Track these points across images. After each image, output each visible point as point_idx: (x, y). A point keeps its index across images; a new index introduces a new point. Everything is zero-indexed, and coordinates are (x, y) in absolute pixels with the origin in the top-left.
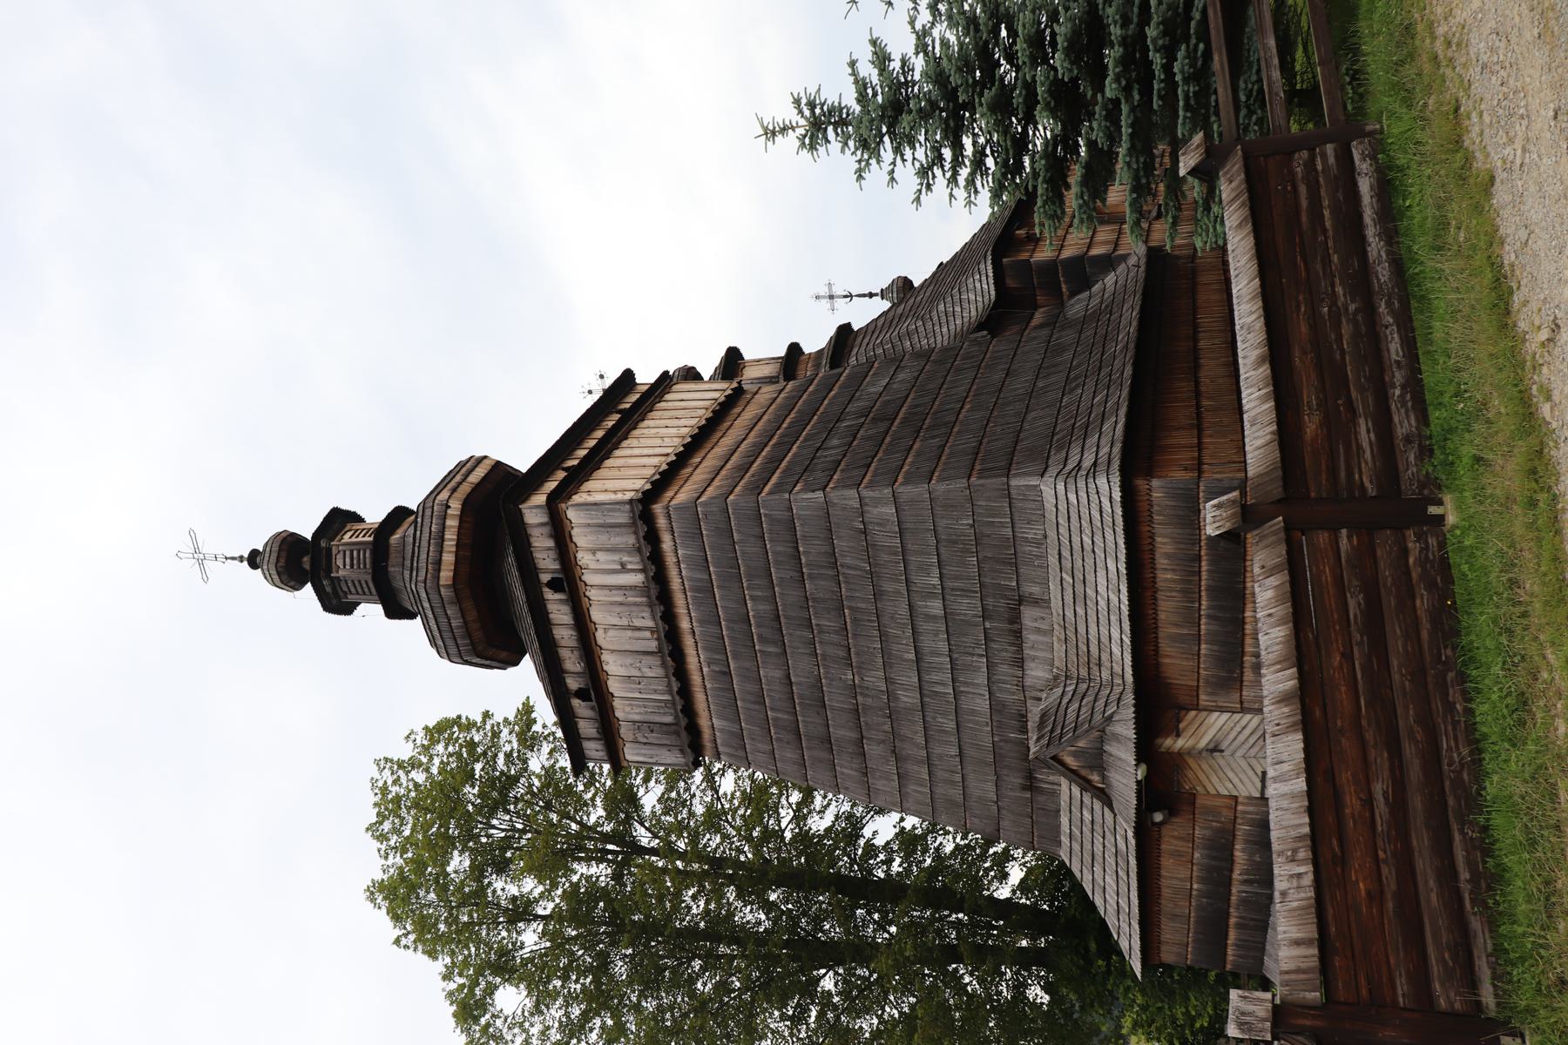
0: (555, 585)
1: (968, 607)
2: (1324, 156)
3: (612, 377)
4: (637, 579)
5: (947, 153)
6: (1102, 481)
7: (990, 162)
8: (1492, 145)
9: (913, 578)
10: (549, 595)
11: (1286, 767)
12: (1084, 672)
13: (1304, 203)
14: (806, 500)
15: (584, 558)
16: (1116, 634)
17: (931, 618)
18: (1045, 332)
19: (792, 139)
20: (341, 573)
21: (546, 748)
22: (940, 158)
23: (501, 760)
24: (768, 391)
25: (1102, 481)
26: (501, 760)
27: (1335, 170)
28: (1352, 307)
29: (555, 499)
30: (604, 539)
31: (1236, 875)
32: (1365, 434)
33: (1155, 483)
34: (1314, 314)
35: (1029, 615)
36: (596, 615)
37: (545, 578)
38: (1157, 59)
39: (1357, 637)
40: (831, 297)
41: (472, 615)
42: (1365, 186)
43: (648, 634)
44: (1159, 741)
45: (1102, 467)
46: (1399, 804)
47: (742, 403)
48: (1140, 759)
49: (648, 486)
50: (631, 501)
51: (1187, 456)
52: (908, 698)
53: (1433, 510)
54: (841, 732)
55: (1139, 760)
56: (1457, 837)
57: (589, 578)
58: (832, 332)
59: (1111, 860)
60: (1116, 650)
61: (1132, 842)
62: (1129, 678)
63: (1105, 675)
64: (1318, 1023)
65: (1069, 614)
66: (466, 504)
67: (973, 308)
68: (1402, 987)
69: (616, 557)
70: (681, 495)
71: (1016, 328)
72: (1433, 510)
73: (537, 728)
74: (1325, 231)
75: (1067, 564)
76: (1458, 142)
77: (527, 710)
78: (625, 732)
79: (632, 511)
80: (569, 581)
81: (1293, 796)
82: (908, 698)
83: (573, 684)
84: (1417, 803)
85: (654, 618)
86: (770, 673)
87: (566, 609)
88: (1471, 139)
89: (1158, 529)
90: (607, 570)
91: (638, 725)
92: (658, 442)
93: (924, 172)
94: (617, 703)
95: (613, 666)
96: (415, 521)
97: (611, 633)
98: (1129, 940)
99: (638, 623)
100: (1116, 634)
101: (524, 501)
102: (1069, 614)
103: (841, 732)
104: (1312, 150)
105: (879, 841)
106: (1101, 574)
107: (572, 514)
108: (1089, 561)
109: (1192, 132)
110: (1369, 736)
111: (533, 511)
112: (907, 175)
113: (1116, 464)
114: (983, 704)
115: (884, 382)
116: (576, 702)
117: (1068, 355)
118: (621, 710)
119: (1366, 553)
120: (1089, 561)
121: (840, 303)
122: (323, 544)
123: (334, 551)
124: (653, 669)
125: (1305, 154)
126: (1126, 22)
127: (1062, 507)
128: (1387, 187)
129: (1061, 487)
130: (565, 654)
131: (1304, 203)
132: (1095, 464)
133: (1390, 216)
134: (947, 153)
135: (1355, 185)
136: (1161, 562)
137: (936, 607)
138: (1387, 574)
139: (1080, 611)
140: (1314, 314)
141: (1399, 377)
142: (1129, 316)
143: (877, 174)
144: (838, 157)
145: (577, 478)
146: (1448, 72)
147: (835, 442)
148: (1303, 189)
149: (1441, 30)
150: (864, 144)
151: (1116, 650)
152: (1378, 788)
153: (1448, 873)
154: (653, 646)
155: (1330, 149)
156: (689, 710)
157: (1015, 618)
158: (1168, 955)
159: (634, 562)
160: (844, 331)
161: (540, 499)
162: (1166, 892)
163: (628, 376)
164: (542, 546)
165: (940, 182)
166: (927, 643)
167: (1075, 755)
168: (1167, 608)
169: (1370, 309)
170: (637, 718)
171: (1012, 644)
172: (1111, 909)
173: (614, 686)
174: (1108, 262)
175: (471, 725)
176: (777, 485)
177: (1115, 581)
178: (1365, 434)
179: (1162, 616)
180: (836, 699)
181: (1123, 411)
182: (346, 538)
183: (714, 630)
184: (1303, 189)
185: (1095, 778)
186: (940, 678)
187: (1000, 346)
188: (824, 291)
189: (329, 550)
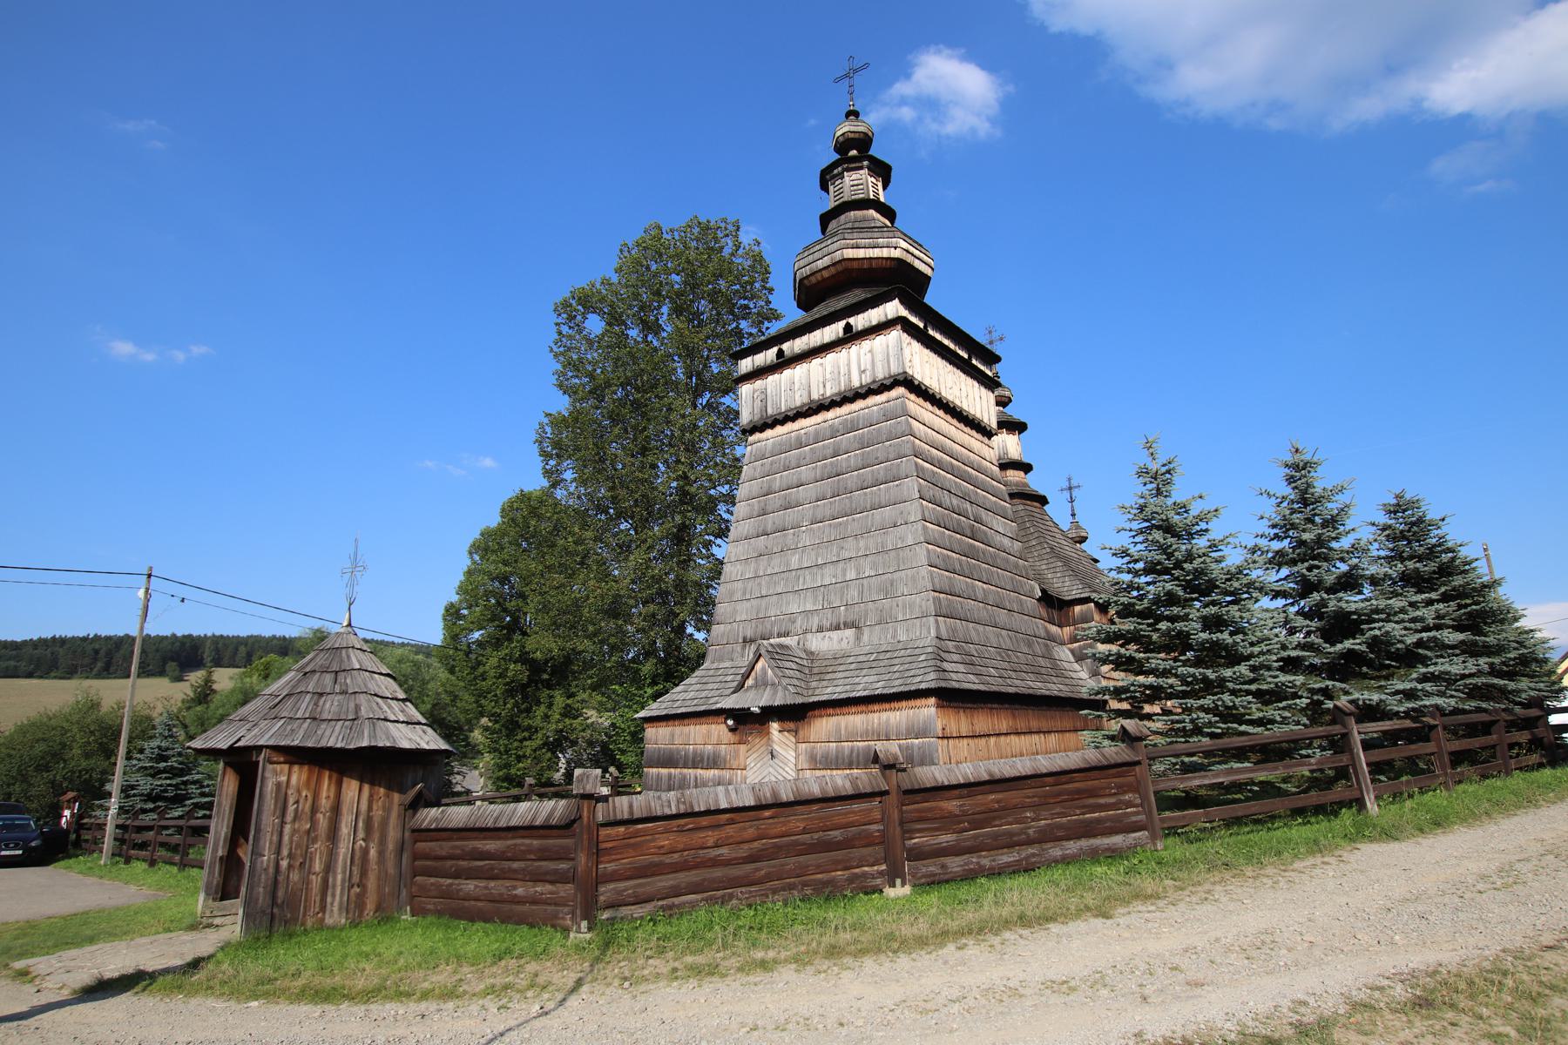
0: (848, 328)
2: (1137, 813)
6: (932, 676)
8: (1130, 918)
9: (869, 559)
10: (842, 324)
11: (733, 795)
12: (815, 670)
13: (1102, 801)
14: (912, 486)
17: (844, 571)
18: (1043, 634)
19: (1143, 459)
20: (847, 179)
21: (754, 331)
22: (1136, 561)
23: (742, 302)
25: (932, 676)
26: (742, 302)
28: (1031, 831)
30: (879, 357)
31: (699, 771)
32: (946, 839)
33: (933, 710)
35: (850, 633)
37: (852, 320)
38: (1208, 701)
39: (816, 836)
41: (826, 274)
42: (1117, 840)
45: (942, 675)
46: (715, 863)
47: (979, 436)
51: (953, 729)
52: (795, 561)
53: (898, 881)
54: (771, 521)
55: (762, 708)
56: (699, 897)
58: (1042, 492)
59: (704, 694)
60: (829, 690)
62: (812, 699)
63: (814, 684)
64: (585, 820)
65: (851, 660)
66: (900, 262)
68: (611, 867)
70: (915, 405)
71: (1045, 615)
72: (898, 881)
73: (766, 324)
76: (1137, 896)
77: (778, 318)
78: (759, 383)
81: (717, 801)
82: (795, 561)
83: (786, 347)
84: (718, 873)
86: (805, 472)
87: (833, 337)
88: (1138, 906)
89: (904, 713)
91: (764, 392)
93: (1124, 553)
94: (776, 376)
98: (654, 709)
99: (828, 386)
100: (838, 689)
101: (902, 302)
102: (851, 660)
103: (771, 521)
104: (1141, 805)
105: (715, 550)
106: (875, 678)
108: (883, 670)
110: (756, 844)
111: (893, 308)
112: (1124, 540)
113: (943, 684)
114: (794, 608)
116: (775, 349)
117: (1025, 650)
118: (772, 379)
119: (869, 841)
120: (883, 670)
124: (799, 400)
125: (1138, 801)
126: (1234, 680)
127: (917, 651)
128: (1114, 854)
129: (930, 650)
130: (805, 338)
131: (1102, 801)
133: (1094, 856)
134: (1140, 565)
135: (1117, 833)
136: (884, 715)
137: (851, 575)
138: (856, 853)
140: (1024, 807)
141: (986, 862)
142: (1055, 688)
144: (1134, 491)
146: (1187, 892)
148: (1112, 800)
149: (1218, 888)
150: (1142, 509)
151: (829, 690)
152: (724, 851)
153: (677, 892)
154: (815, 396)
155: (1142, 817)
156: (772, 425)
157: (847, 625)
158: (651, 732)
159: (867, 379)
160: (1043, 500)
161: (904, 312)
162: (686, 729)
163: (997, 359)
164: (874, 316)
165: (1119, 562)
166: (828, 570)
167: (763, 669)
169: (1030, 842)
172: (675, 697)
173: (787, 373)
175: (765, 281)
176: (923, 468)
178: (946, 839)
179: (851, 718)
180: (791, 515)
181: (982, 688)
183: (828, 434)
184: (1112, 800)
185: (750, 682)
186: (808, 580)
187: (1031, 604)
188: (1074, 483)
189: (861, 168)
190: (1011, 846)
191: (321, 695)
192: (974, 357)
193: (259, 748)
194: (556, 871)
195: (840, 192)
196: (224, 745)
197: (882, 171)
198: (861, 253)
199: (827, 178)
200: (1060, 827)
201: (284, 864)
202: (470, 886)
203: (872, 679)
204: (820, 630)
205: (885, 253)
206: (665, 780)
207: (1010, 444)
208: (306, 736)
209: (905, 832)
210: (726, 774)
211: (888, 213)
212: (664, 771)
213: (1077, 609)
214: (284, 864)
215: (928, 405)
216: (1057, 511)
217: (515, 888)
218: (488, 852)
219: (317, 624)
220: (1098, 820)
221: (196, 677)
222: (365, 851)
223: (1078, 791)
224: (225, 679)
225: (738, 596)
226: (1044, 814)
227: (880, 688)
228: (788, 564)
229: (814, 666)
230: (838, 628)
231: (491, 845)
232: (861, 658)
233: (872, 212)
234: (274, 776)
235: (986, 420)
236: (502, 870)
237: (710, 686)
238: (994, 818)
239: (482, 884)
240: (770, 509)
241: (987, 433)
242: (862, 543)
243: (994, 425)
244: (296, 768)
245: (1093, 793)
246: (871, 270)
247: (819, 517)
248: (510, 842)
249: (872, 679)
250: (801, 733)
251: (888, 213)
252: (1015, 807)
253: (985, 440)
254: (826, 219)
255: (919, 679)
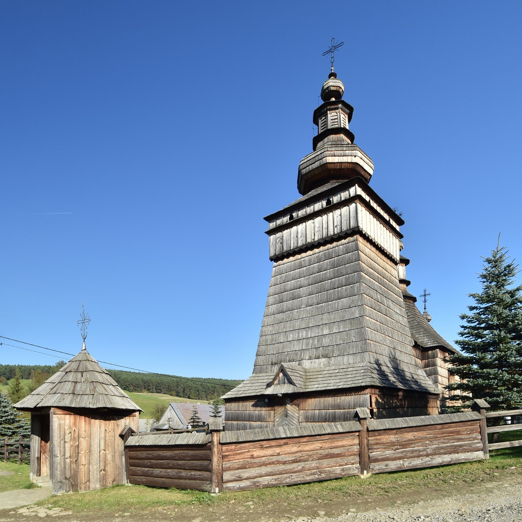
1: (326, 341)
2: (479, 443)
3: (402, 218)
4: (331, 233)
5: (483, 325)
7: (479, 340)
15: (337, 212)
16: (320, 386)
18: (414, 363)
20: (329, 115)
24: (395, 273)
27: (474, 446)
28: (428, 450)
29: (358, 197)
34: (426, 439)
36: (318, 219)
40: (425, 295)
43: (313, 238)
44: (289, 400)
48: (284, 395)
49: (364, 233)
50: (358, 227)
54: (285, 305)
57: (331, 214)
58: (414, 296)
60: (316, 386)
61: (259, 394)
62: (307, 390)
65: (325, 372)
67: (422, 340)
69: (339, 224)
74: (453, 443)
75: (341, 371)
78: (279, 235)
79: (355, 228)
80: (331, 208)
85: (319, 240)
87: (320, 208)
90: (333, 222)
92: (379, 235)
95: (301, 227)
96: (349, 144)
97: (313, 225)
99: (317, 235)
100: (320, 386)
102: (325, 372)
106: (338, 381)
107: (353, 205)
109: (489, 403)
111: (356, 190)
115: (398, 312)
118: (286, 232)
121: (423, 298)
122: (340, 105)
123: (337, 111)
132: (373, 377)
137: (326, 332)
139: (327, 375)
143: (474, 303)
145: (367, 205)
147: (379, 296)
151: (316, 386)
154: (309, 240)
157: (325, 356)
160: (414, 300)
161: (360, 191)
168: (330, 400)
169: (427, 455)
170: (285, 238)
171: (315, 356)
173: (294, 228)
174: (436, 382)
177: (337, 384)
179: (326, 399)
182: (342, 116)
185: (276, 382)
188: (427, 293)
189: (337, 108)
190: (418, 456)
191: (76, 382)
192: (392, 219)
193: (49, 408)
194: (178, 465)
195: (326, 123)
196: (32, 405)
197: (350, 111)
198: (336, 160)
199: (319, 114)
200: (442, 448)
201: (68, 461)
202: (157, 471)
203: (337, 381)
204: (310, 358)
205: (349, 159)
206: (235, 426)
207: (402, 271)
208: (71, 402)
209: (369, 449)
210: (264, 424)
211: (350, 136)
212: (235, 422)
213: (430, 352)
214: (68, 461)
215: (368, 245)
216: (419, 305)
217: (181, 473)
218: (166, 456)
219: (62, 360)
220: (460, 446)
221: (12, 382)
222: (105, 455)
223: (452, 432)
224: (25, 383)
225: (269, 342)
226: (435, 442)
227: (342, 385)
228: (294, 326)
229: (307, 375)
230: (319, 358)
231: (144, 454)
232: (330, 372)
233: (342, 136)
234: (59, 422)
235: (395, 256)
236: (173, 464)
237: (256, 385)
238: (411, 444)
239: (164, 470)
240: (285, 299)
241: (396, 263)
242: (333, 316)
243: (398, 258)
244: (67, 417)
245: (458, 433)
246: (341, 169)
247: (310, 303)
248: (176, 452)
249: (337, 381)
250: (301, 406)
251: (350, 136)
252: (422, 439)
253: (393, 265)
254: (317, 140)
255: (361, 381)
